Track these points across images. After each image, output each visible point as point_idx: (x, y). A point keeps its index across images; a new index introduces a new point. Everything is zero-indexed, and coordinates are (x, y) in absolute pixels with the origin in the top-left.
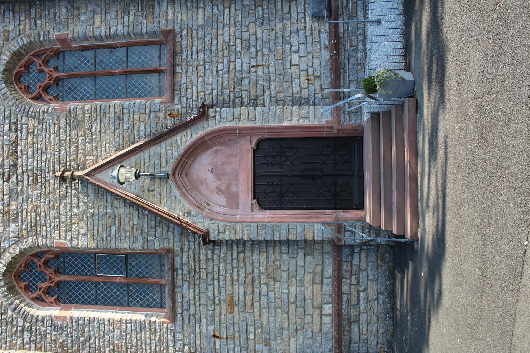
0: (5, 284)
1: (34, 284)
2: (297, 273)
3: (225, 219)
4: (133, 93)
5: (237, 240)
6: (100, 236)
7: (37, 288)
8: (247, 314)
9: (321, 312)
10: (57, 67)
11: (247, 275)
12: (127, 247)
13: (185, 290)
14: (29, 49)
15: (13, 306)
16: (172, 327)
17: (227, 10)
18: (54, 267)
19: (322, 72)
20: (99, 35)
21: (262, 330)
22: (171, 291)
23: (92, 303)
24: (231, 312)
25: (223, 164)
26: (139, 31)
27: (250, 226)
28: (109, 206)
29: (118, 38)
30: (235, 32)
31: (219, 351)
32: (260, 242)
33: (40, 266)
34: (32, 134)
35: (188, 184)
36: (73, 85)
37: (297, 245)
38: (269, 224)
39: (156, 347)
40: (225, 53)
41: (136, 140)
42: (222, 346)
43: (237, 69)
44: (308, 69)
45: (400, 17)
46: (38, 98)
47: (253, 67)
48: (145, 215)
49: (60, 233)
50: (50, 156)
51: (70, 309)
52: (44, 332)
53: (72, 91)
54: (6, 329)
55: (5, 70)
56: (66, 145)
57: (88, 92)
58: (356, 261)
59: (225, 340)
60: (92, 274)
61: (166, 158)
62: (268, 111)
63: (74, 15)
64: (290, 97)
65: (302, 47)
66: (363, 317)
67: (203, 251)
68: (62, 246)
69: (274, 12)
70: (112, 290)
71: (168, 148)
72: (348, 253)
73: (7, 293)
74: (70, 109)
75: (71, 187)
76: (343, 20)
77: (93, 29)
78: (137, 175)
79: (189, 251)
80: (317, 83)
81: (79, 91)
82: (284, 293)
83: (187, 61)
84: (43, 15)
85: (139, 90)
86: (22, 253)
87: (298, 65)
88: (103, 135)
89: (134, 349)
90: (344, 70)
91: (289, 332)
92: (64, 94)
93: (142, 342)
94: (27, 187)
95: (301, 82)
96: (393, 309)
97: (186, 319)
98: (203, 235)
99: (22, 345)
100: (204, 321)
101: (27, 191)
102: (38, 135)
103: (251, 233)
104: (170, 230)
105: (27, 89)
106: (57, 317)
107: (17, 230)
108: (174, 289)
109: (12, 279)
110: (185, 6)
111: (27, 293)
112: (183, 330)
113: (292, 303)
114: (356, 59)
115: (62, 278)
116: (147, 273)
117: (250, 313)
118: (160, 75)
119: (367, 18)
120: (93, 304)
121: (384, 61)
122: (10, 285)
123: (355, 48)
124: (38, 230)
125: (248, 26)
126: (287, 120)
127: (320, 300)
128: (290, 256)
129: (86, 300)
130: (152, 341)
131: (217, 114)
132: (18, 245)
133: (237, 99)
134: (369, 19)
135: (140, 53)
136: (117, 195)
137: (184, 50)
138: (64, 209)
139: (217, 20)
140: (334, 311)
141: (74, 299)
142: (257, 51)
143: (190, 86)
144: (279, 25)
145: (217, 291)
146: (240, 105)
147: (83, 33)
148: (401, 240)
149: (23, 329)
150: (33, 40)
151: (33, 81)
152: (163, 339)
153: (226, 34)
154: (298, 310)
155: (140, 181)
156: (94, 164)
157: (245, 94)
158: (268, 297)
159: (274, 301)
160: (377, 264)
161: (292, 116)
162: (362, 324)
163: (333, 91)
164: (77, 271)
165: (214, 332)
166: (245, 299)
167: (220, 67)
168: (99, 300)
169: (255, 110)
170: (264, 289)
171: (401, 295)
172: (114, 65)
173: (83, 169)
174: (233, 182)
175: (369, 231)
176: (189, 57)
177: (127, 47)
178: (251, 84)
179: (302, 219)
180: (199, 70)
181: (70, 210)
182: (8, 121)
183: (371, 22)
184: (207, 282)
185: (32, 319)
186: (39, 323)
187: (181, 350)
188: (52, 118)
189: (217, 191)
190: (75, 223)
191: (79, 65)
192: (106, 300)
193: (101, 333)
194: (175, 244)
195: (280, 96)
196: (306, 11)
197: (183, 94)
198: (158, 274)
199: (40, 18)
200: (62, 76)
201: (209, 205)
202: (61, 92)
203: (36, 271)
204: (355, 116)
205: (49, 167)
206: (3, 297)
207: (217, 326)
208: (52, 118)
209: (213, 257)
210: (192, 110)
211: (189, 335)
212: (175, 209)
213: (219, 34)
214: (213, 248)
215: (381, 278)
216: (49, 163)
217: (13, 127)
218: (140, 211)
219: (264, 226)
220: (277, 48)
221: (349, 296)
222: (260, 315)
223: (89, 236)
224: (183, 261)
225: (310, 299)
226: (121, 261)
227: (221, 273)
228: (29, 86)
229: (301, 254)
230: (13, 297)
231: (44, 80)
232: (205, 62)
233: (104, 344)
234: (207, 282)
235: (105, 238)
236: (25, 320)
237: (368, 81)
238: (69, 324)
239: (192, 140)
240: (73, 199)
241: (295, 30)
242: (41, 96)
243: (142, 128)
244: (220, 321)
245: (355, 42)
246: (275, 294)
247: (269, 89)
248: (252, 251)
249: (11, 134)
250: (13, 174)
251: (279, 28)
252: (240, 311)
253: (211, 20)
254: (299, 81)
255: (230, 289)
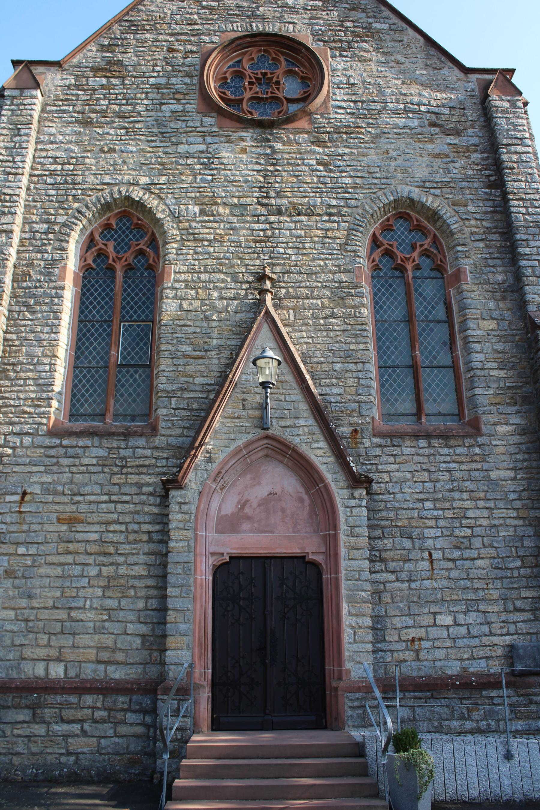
0: (115, 200)
1: (112, 236)
2: (116, 623)
3: (200, 513)
4: (386, 377)
5: (169, 531)
6: (179, 328)
7: (107, 240)
8: (56, 544)
9: (53, 660)
10: (420, 269)
11: (115, 545)
12: (162, 368)
13: (95, 452)
14: (444, 232)
15: (84, 210)
16: (41, 431)
17: (514, 514)
18: (135, 264)
19: (426, 663)
20: (468, 327)
21: (30, 566)
22: (94, 430)
23: (82, 316)
24: (59, 520)
25: (283, 510)
26: (476, 384)
27: (189, 552)
28: (222, 342)
29: (466, 354)
30: (481, 526)
31: (2, 500)
32: (165, 565)
33: (138, 245)
34: (325, 235)
35: (253, 457)
36: (395, 290)
37: (158, 623)
38: (192, 580)
39: (13, 406)
40: (449, 511)
41: (318, 381)
42: (9, 505)
43: (426, 531)
44: (429, 640)
45: (520, 794)
46: (375, 242)
47: (430, 554)
48: (208, 395)
49: (184, 272)
50: (293, 259)
51: (75, 285)
52: (45, 250)
53: (387, 290)
54: (53, 201)
55: (412, 200)
56: (309, 281)
57: (385, 312)
58: (131, 717)
59: (17, 509)
60: (123, 317)
61: (291, 426)
62: (363, 578)
63: (494, 292)
64: (386, 612)
65: (463, 630)
66: (40, 729)
67: (152, 479)
68: (166, 276)
69: (516, 585)
70: (99, 344)
71: (306, 429)
72: (144, 705)
73: (103, 201)
74: (361, 287)
75: (250, 288)
76: (507, 697)
77: (476, 319)
78: (267, 385)
79: (154, 458)
80: (408, 655)
81: (388, 299)
82: (86, 601)
83: (435, 455)
84: (491, 250)
85: (391, 385)
86: (157, 222)
87: (435, 625)
88: (324, 334)
89: (12, 374)
90: (430, 698)
91: (25, 608)
92: (382, 278)
93: (21, 386)
94: (249, 229)
95: (410, 630)
96: (50, 781)
97: (53, 452)
98: (177, 480)
99: (30, 221)
100: (48, 479)
101: (244, 228)
102: (324, 244)
103: (179, 552)
104: (185, 431)
105: (387, 228)
106: (65, 268)
107: (189, 215)
108: (97, 435)
109: (121, 207)
110: (516, 451)
111: (101, 227)
112: (35, 447)
113: (69, 614)
114: (449, 717)
115: (119, 275)
116: (122, 395)
117: (58, 548)
118: (413, 415)
119: (514, 737)
120: (80, 316)
121: (447, 765)
122: (113, 206)
123: (466, 716)
124: (188, 243)
125: (491, 546)
126: (350, 608)
127: (72, 658)
128: (143, 612)
129: (87, 307)
130: (22, 402)
131: (357, 501)
132: (169, 216)
133: (381, 530)
134: (512, 740)
135: (445, 385)
136: (238, 354)
137: (451, 451)
138: (217, 279)
139: (498, 499)
140: (53, 681)
141: (88, 290)
142: (454, 560)
143: (398, 460)
144: (495, 594)
145: (92, 500)
146: (372, 536)
147: (470, 305)
148: (164, 794)
149: (51, 222)
150: (456, 237)
151: (399, 237)
152: (25, 418)
153: (478, 513)
154: (58, 623)
155: (257, 387)
156: (282, 321)
157: (388, 543)
158: (80, 576)
159: (73, 586)
160: (124, 754)
161: (356, 615)
162: (29, 727)
163: (395, 680)
164: (129, 294)
165: (31, 493)
166: (79, 542)
167: (428, 505)
168: (85, 326)
169: (365, 559)
170: (93, 571)
171: (74, 794)
172: (426, 348)
173: (275, 306)
174: (256, 525)
175: (177, 740)
176: (442, 458)
177: (453, 367)
178: (404, 552)
179: (199, 632)
180: (423, 473)
181: (217, 287)
182: (342, 204)
183: (507, 742)
184: (106, 485)
185: (65, 234)
186: (57, 244)
187: (7, 443)
188: (347, 262)
189: (243, 502)
190: (197, 293)
191: (425, 299)
192: (84, 335)
193: (39, 329)
194: (164, 439)
195: (386, 598)
196: (520, 637)
197: (386, 450)
198: (121, 411)
199: (488, 247)
200: (408, 276)
201: (222, 489)
202: (385, 273)
203: (130, 240)
204: (359, 716)
205: (278, 258)
206: (97, 197)
207: (40, 498)
208: (347, 262)
209: (143, 494)
210: (363, 464)
211: (28, 456)
212: (216, 438)
213: (478, 502)
214: (158, 494)
215: (101, 759)
216: (283, 259)
217: (333, 211)
218: (214, 387)
219: (188, 572)
220: (460, 592)
221: (75, 706)
222: (53, 564)
223: (179, 313)
224: (139, 450)
225: (74, 642)
226: (141, 358)
227: (119, 506)
228: (392, 230)
229: (144, 629)
230: (97, 209)
231: (401, 251)
232: (435, 481)
233: (22, 332)
234: (106, 485)
235: (174, 336)
236: (64, 225)
237: (413, 738)
238: (54, 284)
239: (318, 464)
240: (232, 291)
241: (489, 620)
242: (379, 247)
243: (335, 390)
244: (46, 503)
245: (475, 715)
246: (84, 587)
247: (397, 580)
248: (151, 553)
249: (324, 207)
250: (268, 210)
251: (490, 594)
252: (61, 534)
253: (498, 489)
254: (410, 627)
255: (95, 519)
